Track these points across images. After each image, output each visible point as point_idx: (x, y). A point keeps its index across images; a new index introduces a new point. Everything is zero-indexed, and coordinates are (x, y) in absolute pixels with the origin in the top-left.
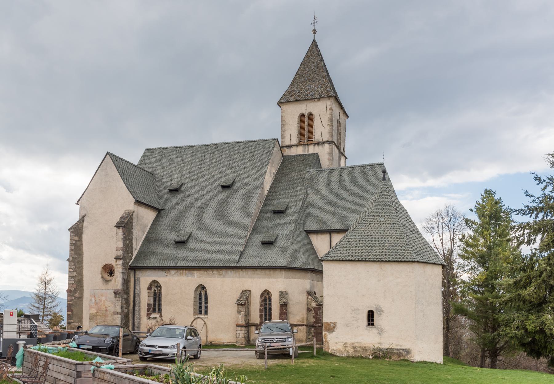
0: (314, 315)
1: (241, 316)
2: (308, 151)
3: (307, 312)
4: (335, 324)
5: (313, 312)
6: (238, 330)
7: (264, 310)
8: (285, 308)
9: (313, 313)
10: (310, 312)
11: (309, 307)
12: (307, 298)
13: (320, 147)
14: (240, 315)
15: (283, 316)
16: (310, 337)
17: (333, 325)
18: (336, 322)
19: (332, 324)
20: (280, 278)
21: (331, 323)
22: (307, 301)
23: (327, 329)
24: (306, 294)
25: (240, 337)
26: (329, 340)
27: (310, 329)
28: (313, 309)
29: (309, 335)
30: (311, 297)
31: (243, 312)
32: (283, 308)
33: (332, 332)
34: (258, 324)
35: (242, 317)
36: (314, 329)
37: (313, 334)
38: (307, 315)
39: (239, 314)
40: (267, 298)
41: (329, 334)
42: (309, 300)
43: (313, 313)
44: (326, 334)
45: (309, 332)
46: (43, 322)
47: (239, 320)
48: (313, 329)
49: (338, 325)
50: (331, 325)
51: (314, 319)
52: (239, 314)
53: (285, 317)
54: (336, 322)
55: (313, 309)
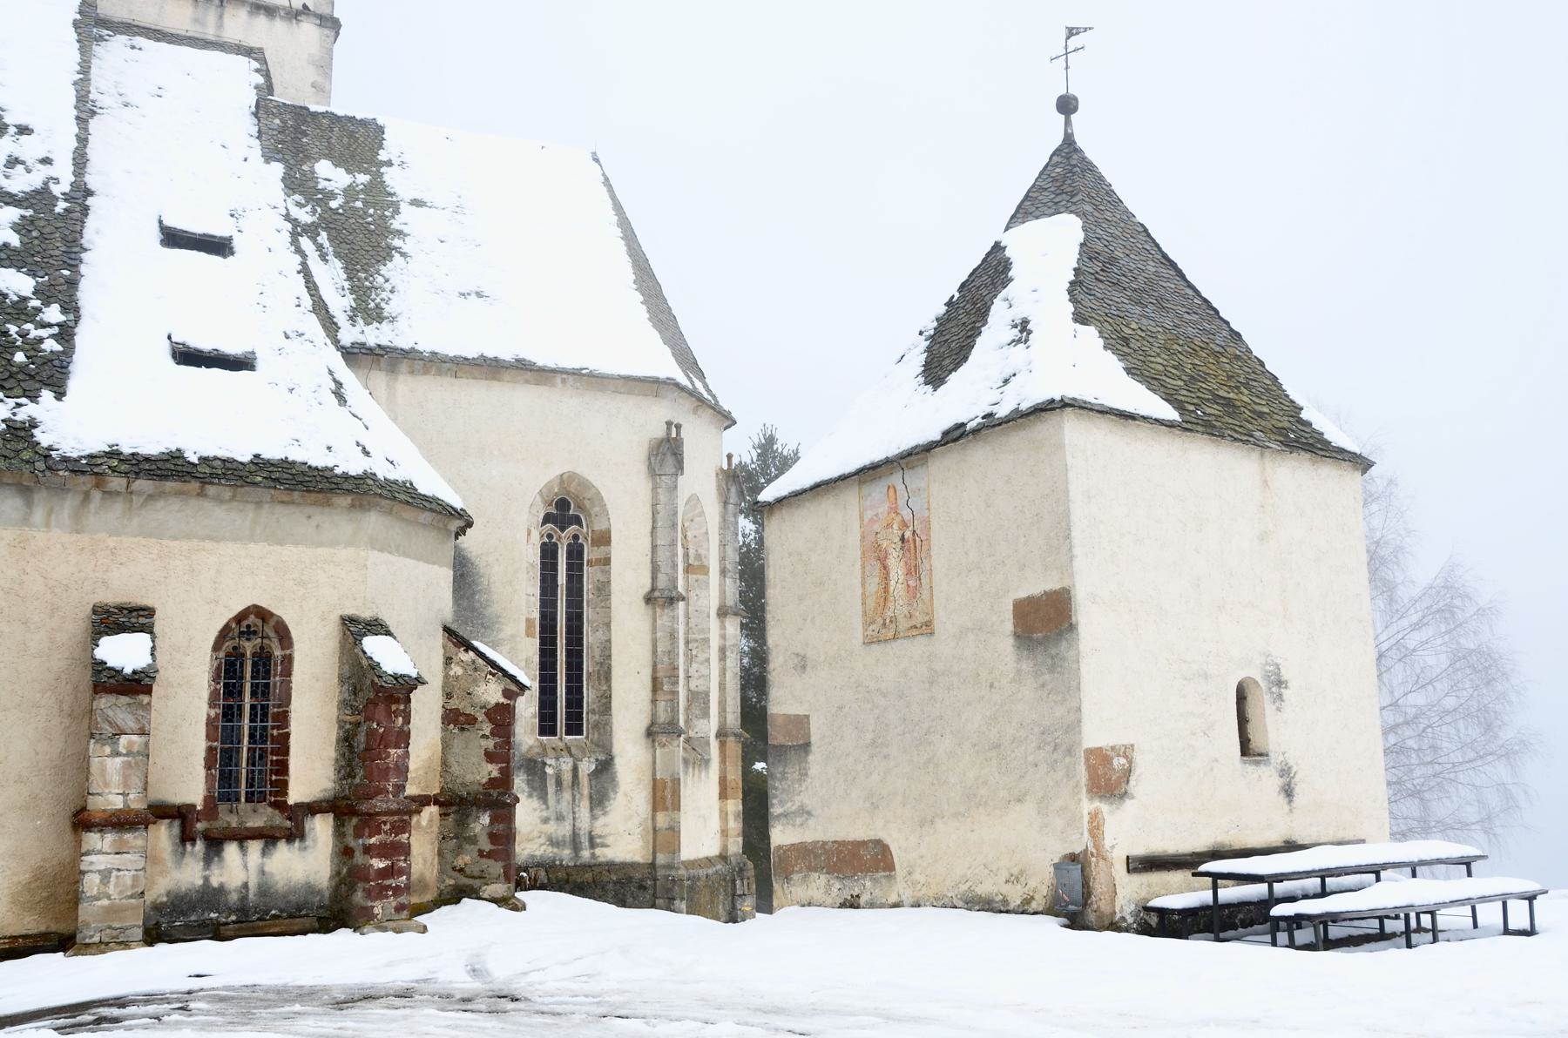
0: (490, 744)
1: (118, 760)
2: (220, 26)
3: (444, 730)
4: (1127, 751)
5: (487, 728)
6: (100, 852)
7: (221, 724)
8: (402, 707)
9: (484, 736)
10: (462, 729)
11: (454, 704)
12: (448, 661)
13: (279, 25)
14: (117, 754)
15: (388, 755)
16: (464, 859)
17: (1123, 761)
18: (1132, 745)
19: (1119, 755)
20: (349, 544)
21: (1113, 748)
22: (446, 677)
23: (1099, 787)
24: (439, 637)
25: (109, 897)
26: (1113, 847)
27: (462, 823)
28: (481, 717)
29: (458, 851)
30: (471, 653)
31: (135, 738)
32: (394, 707)
33: (1124, 795)
34: (194, 806)
35: (127, 765)
36: (493, 821)
37: (486, 846)
38: (446, 745)
39: (108, 750)
40: (243, 655)
41: (1111, 812)
42: (457, 670)
43: (484, 736)
44: (1096, 814)
45: (456, 837)
46: (592, 728)
47: (106, 785)
48: (485, 819)
49: (1143, 765)
50: (1115, 762)
51: (490, 767)
52: (108, 750)
53: (398, 756)
54: (1132, 745)
55: (481, 717)
